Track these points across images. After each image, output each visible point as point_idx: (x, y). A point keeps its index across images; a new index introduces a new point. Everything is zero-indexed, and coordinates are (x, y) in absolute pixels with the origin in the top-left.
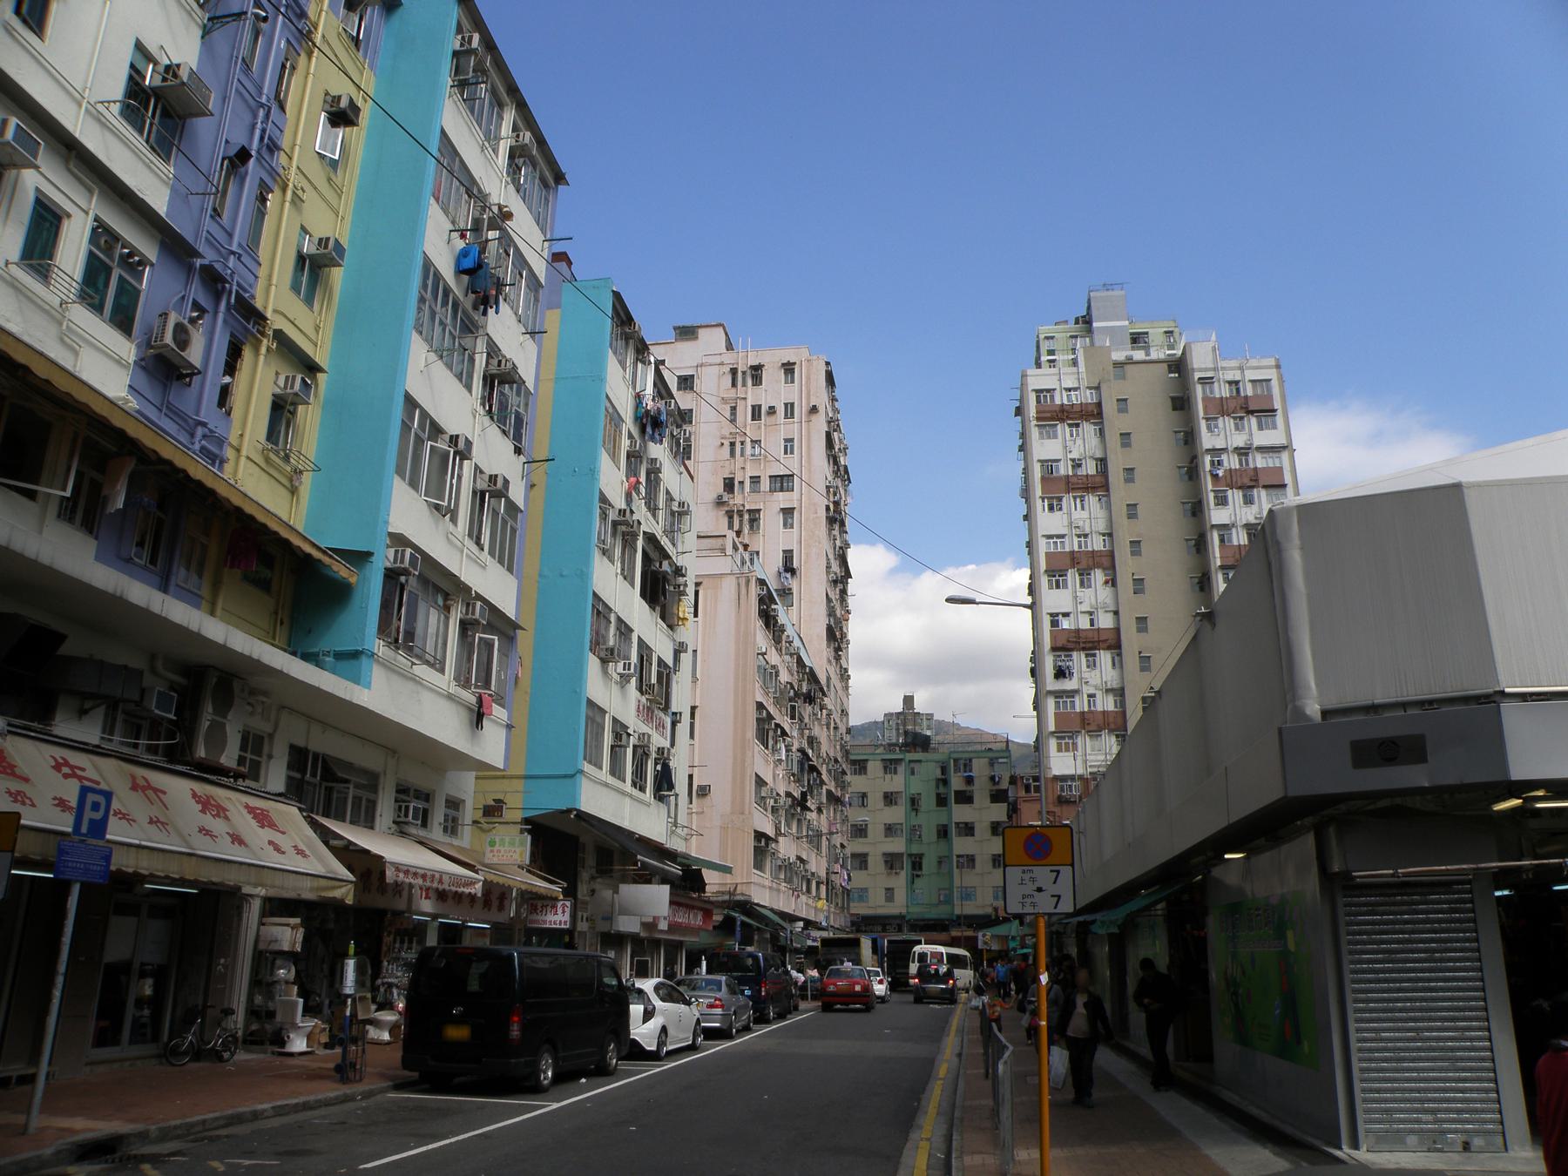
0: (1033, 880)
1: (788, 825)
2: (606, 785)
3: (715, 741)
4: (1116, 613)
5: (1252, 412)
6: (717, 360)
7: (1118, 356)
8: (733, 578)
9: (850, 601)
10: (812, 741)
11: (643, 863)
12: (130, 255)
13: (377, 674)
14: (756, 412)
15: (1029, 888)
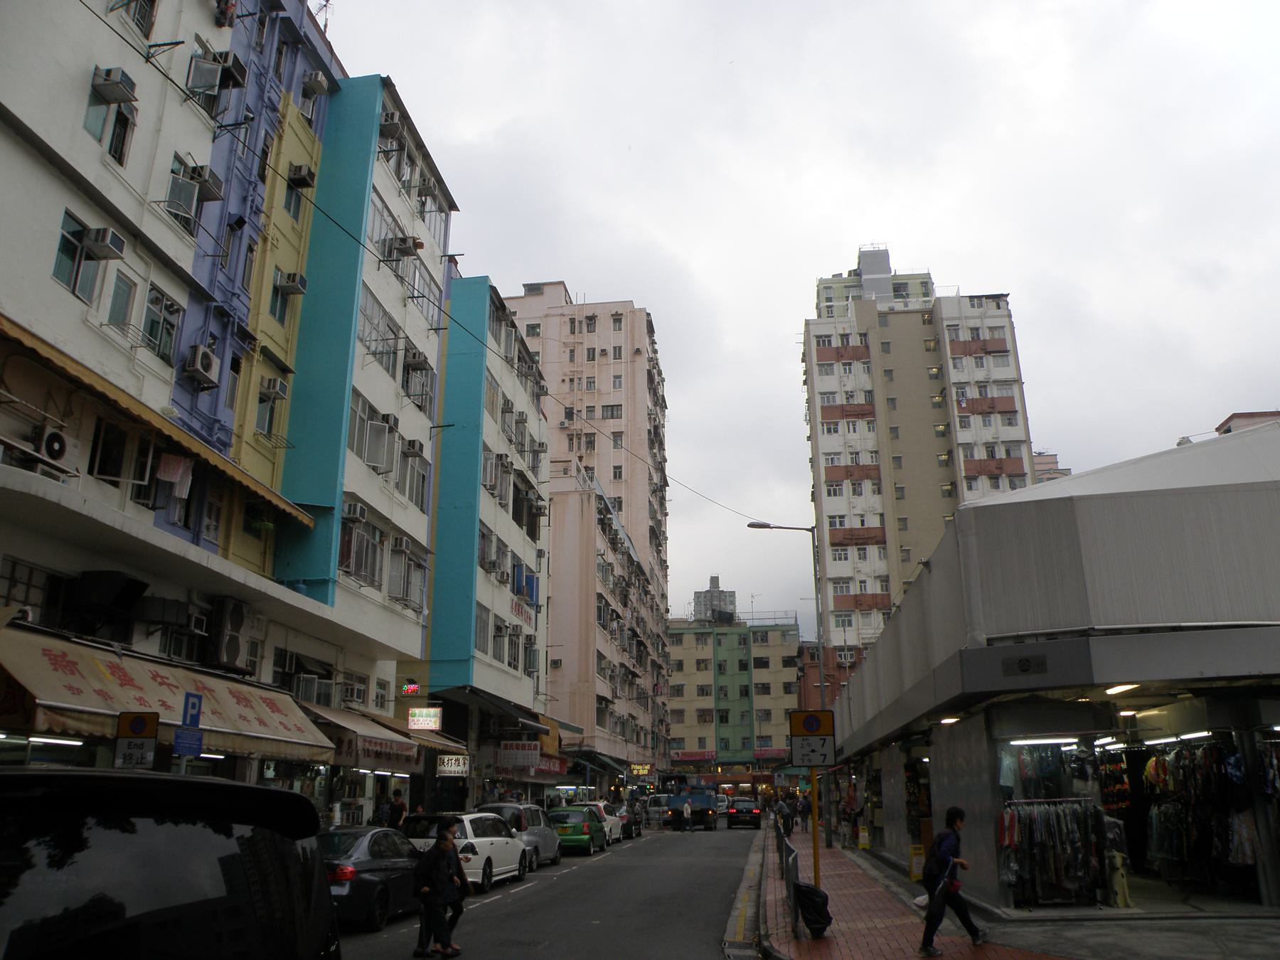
0: (809, 745)
1: (622, 690)
2: (490, 666)
3: (564, 620)
4: (882, 515)
5: (989, 353)
6: (560, 312)
7: (883, 307)
8: (577, 496)
9: (668, 504)
10: (640, 621)
11: (523, 724)
12: (172, 305)
13: (338, 596)
14: (591, 354)
15: (807, 750)
